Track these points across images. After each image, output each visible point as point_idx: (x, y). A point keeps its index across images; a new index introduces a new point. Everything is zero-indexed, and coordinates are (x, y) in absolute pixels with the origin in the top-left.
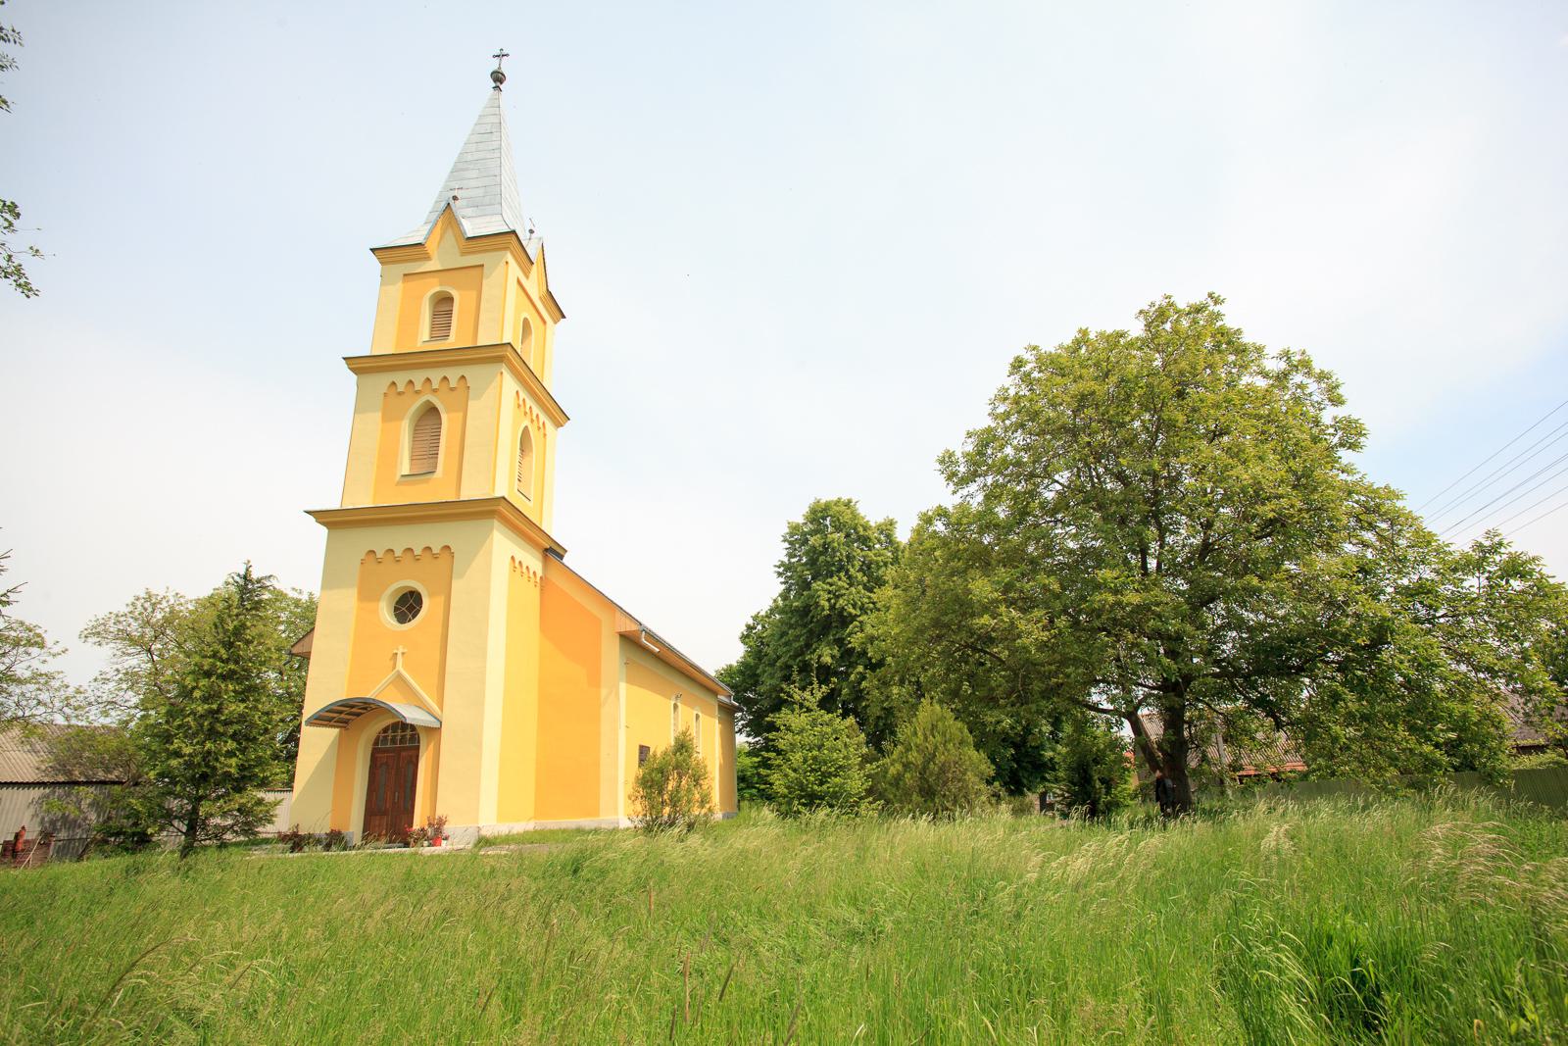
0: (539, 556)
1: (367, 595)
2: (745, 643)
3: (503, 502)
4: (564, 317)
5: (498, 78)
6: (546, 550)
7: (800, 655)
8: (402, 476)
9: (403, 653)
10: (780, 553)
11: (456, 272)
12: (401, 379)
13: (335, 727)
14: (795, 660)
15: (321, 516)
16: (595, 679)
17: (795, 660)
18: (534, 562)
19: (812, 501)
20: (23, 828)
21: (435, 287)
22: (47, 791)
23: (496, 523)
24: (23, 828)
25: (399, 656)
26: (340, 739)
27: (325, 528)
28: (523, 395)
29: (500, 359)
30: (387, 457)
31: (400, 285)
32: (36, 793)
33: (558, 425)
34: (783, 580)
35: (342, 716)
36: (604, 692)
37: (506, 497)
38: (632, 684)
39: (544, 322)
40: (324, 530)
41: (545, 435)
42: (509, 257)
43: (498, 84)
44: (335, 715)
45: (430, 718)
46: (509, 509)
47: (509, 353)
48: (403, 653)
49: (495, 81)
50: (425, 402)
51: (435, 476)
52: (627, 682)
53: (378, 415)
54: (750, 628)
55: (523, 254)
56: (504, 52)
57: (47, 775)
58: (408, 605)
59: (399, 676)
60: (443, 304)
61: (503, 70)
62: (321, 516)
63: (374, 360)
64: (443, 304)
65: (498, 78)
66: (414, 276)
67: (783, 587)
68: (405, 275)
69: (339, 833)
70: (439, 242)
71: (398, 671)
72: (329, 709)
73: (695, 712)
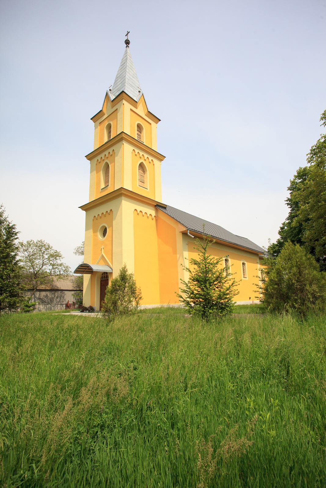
0: (153, 208)
1: (95, 231)
2: (280, 234)
3: (122, 189)
4: (160, 120)
5: (127, 42)
6: (155, 206)
7: (297, 236)
8: (102, 189)
9: (103, 248)
10: (287, 194)
11: (111, 115)
12: (99, 158)
13: (89, 274)
14: (295, 238)
15: (82, 207)
16: (175, 252)
17: (295, 238)
18: (151, 212)
19: (298, 169)
20: (68, 301)
21: (106, 123)
22: (75, 292)
23: (123, 198)
24: (68, 301)
25: (102, 249)
26: (91, 276)
27: (85, 211)
28: (137, 151)
29: (122, 139)
30: (98, 183)
31: (99, 127)
32: (73, 292)
33: (161, 160)
34: (290, 206)
35: (87, 270)
36: (178, 256)
37: (122, 187)
38: (191, 251)
39: (150, 124)
40: (84, 212)
41: (154, 164)
42: (124, 102)
43: (128, 45)
44: (85, 270)
45: (110, 269)
46: (134, 194)
47: (123, 135)
48: (103, 248)
49: (126, 44)
50: (105, 164)
51: (109, 186)
52: (189, 251)
53: (95, 171)
54: (282, 228)
55: (131, 100)
56: (128, 32)
57: (75, 288)
58: (105, 232)
59: (103, 256)
60: (109, 127)
61: (129, 39)
62: (82, 207)
63: (92, 154)
64: (109, 127)
65: (127, 42)
66: (102, 122)
67: (291, 209)
68: (100, 123)
69: (92, 307)
70: (106, 108)
71: (102, 254)
72: (78, 268)
73: (242, 262)
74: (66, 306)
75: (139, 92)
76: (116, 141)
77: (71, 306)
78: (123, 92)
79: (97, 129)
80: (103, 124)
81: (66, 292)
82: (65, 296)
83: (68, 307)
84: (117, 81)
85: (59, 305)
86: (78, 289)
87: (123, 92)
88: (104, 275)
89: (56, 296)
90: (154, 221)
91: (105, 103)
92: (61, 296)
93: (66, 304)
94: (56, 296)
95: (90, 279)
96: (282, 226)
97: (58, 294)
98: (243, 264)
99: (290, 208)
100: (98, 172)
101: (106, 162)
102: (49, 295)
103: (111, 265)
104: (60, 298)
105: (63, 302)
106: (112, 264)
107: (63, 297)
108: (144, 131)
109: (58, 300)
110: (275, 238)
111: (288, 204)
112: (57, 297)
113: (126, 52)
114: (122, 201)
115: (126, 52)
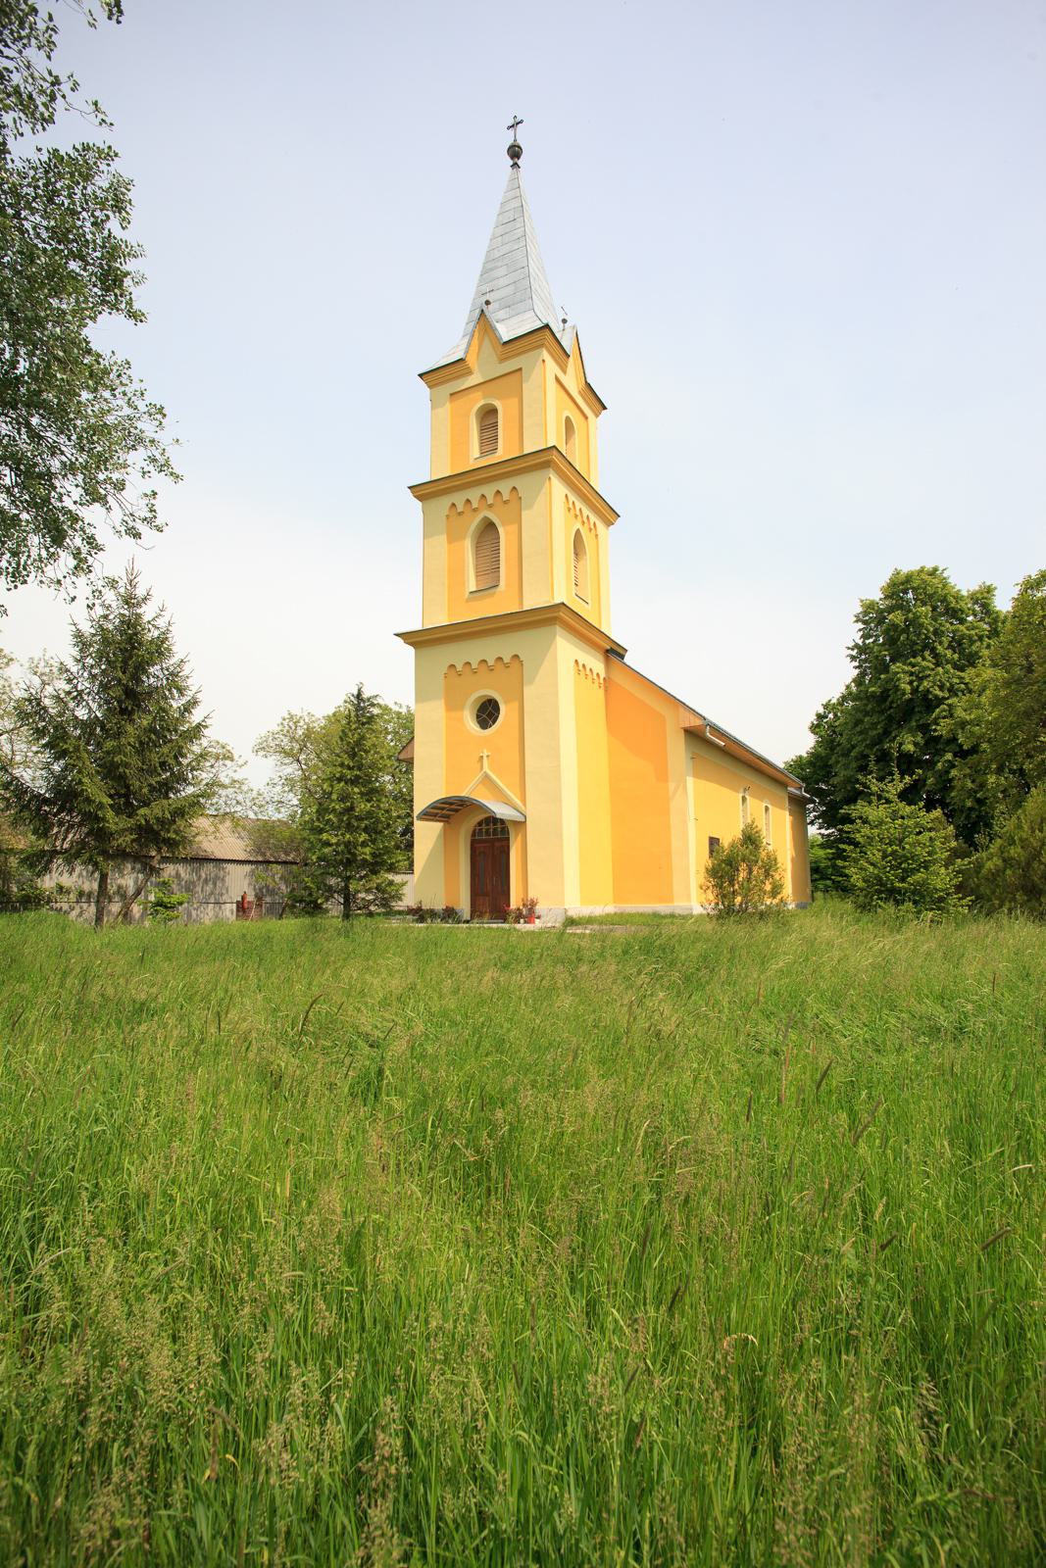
0: (601, 657)
3: (563, 608)
5: (515, 152)
6: (607, 651)
10: (853, 634)
12: (459, 499)
15: (408, 637)
16: (662, 775)
18: (596, 664)
21: (479, 401)
23: (558, 629)
26: (445, 830)
28: (572, 498)
29: (546, 465)
30: (455, 573)
32: (248, 868)
34: (857, 664)
36: (672, 786)
39: (586, 418)
40: (411, 650)
41: (597, 535)
42: (545, 355)
47: (555, 457)
49: (512, 158)
51: (499, 589)
54: (820, 717)
56: (518, 120)
58: (488, 712)
59: (487, 777)
61: (520, 142)
62: (408, 637)
67: (857, 671)
72: (433, 806)
74: (238, 907)
75: (564, 321)
76: (535, 465)
77: (250, 909)
78: (547, 326)
79: (440, 410)
80: (461, 401)
81: (230, 867)
82: (227, 879)
83: (244, 912)
84: (491, 270)
85: (211, 906)
86: (260, 859)
87: (547, 326)
88: (484, 827)
89: (204, 876)
90: (602, 691)
91: (476, 341)
92: (217, 878)
93: (238, 902)
94: (204, 876)
95: (439, 836)
96: (821, 711)
97: (208, 869)
98: (767, 809)
99: (856, 667)
100: (453, 537)
101: (486, 518)
102: (183, 875)
103: (519, 803)
104: (215, 884)
105: (222, 895)
106: (525, 805)
107: (223, 880)
108: (577, 437)
109: (209, 888)
110: (804, 744)
111: (853, 658)
112: (206, 881)
113: (515, 186)
114: (555, 636)
115: (515, 186)
